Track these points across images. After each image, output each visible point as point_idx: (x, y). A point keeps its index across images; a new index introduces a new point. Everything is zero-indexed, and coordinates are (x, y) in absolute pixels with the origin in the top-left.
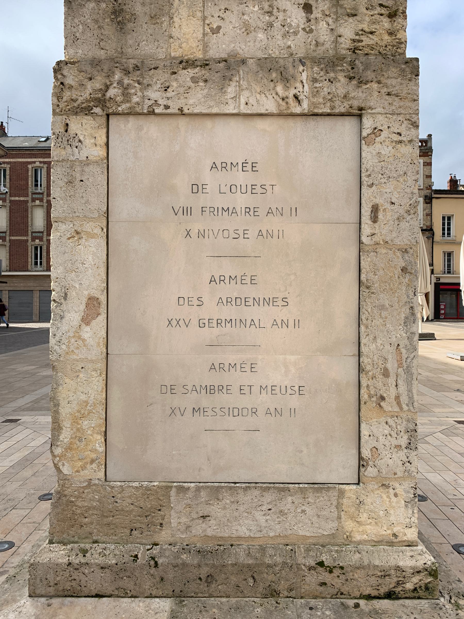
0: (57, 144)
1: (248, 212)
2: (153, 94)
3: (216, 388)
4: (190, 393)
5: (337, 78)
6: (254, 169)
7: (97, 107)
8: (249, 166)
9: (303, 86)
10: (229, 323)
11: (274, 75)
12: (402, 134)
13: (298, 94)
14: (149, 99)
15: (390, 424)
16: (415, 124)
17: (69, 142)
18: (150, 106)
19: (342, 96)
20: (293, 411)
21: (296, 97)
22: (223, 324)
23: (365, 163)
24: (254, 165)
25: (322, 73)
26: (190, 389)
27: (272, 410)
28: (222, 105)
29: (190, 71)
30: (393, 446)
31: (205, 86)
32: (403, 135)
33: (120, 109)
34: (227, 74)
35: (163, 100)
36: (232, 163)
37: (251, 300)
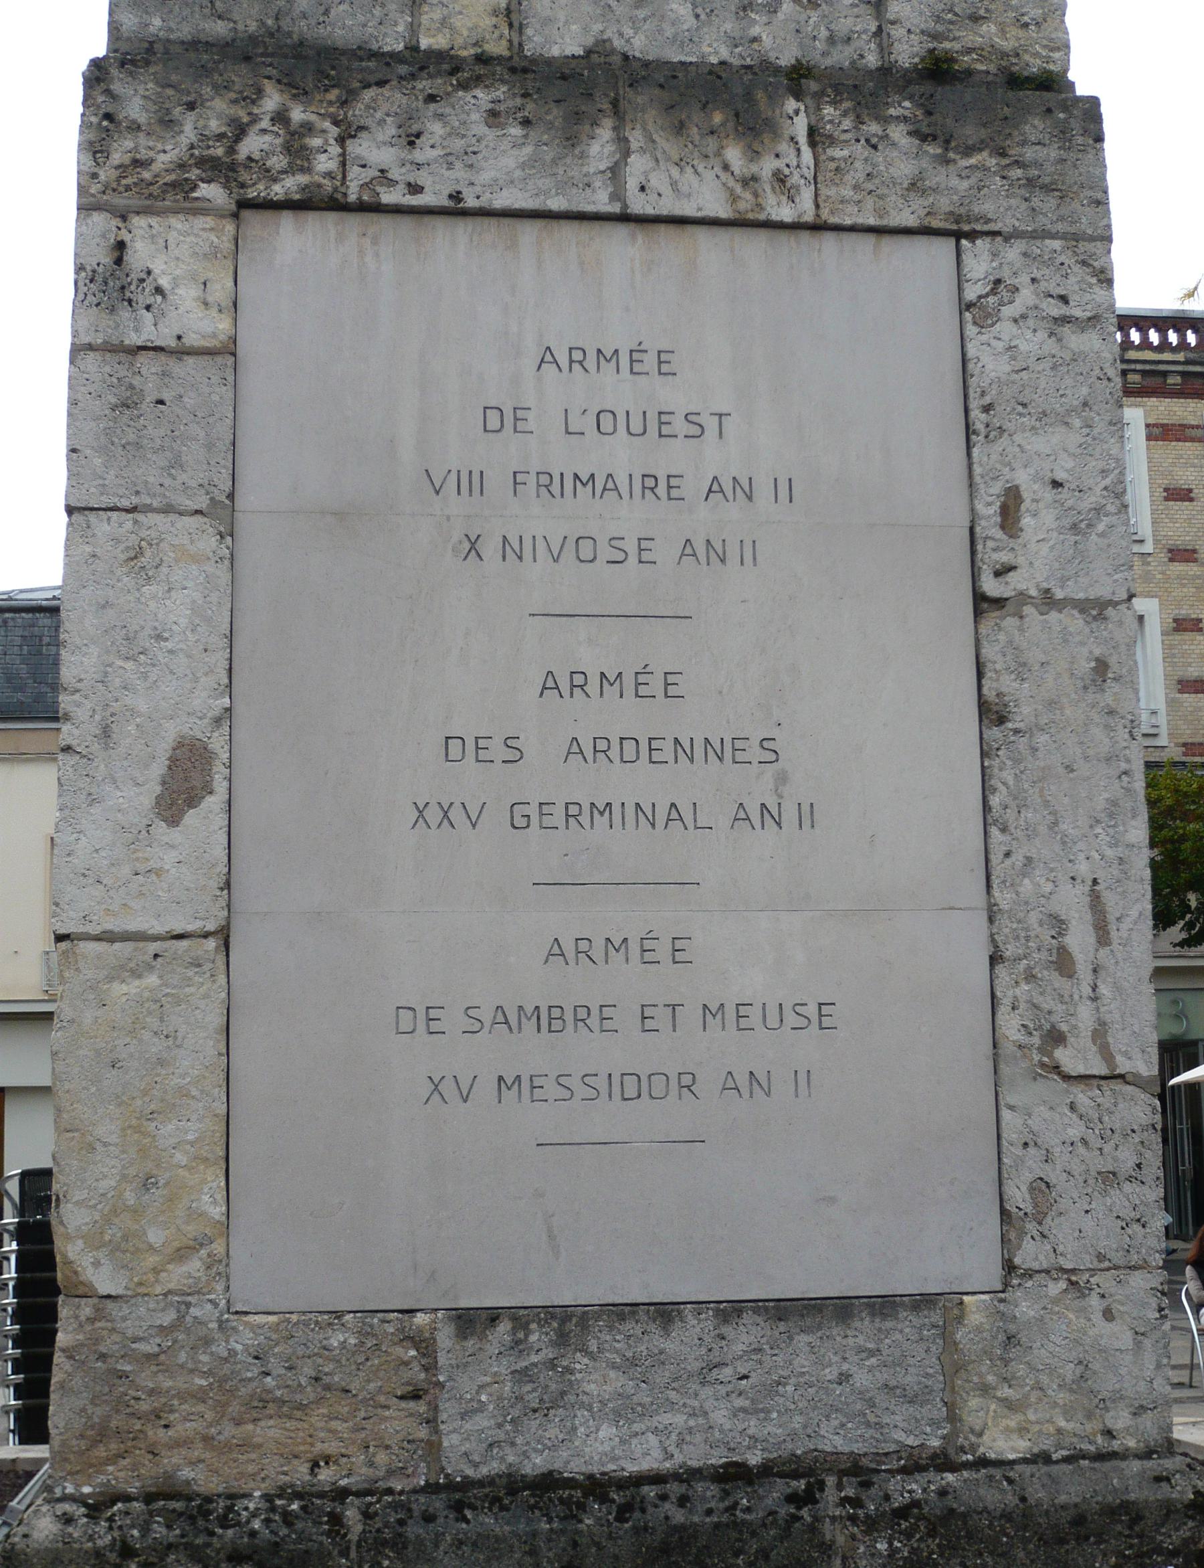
0: (90, 298)
1: (652, 489)
2: (375, 151)
3: (569, 1017)
4: (486, 1029)
5: (887, 135)
6: (665, 368)
7: (209, 182)
8: (650, 361)
9: (798, 150)
10: (602, 813)
11: (718, 118)
12: (1071, 298)
13: (787, 171)
14: (364, 166)
15: (1082, 1110)
16: (1102, 277)
17: (128, 294)
18: (367, 184)
19: (905, 186)
20: (802, 1077)
21: (780, 179)
22: (585, 819)
23: (977, 372)
24: (664, 357)
25: (847, 123)
26: (487, 1019)
27: (742, 1080)
28: (574, 190)
29: (480, 95)
30: (1094, 1173)
31: (526, 136)
32: (1072, 303)
33: (277, 188)
34: (583, 108)
35: (403, 170)
36: (599, 351)
37: (669, 745)
